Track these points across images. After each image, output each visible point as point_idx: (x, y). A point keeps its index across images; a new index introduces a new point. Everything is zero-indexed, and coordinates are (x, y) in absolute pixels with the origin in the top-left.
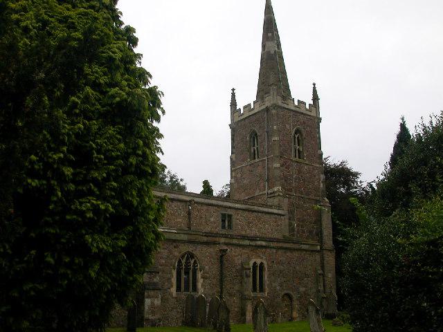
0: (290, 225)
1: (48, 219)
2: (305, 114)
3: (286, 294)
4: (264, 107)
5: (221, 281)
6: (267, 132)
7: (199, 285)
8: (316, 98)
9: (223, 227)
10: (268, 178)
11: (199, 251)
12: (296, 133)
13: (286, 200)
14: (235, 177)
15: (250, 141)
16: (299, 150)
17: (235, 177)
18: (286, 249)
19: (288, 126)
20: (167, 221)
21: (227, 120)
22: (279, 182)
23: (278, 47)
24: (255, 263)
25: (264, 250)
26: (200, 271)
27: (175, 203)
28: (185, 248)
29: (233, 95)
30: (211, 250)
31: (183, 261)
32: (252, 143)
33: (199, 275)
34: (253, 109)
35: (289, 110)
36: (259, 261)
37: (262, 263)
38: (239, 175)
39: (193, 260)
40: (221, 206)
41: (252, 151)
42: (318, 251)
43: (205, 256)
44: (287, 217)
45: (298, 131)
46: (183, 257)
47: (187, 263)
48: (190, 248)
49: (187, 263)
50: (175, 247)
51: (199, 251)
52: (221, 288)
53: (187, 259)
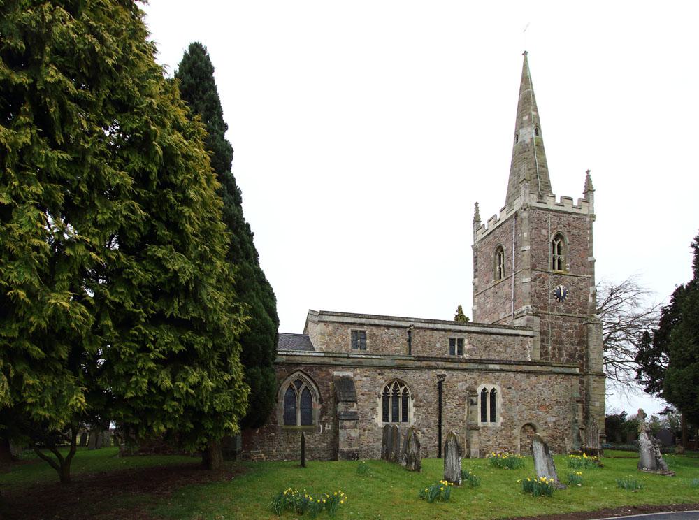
0: (543, 347)
1: (121, 413)
2: (570, 213)
3: (528, 424)
4: (512, 213)
5: (440, 400)
6: (515, 243)
7: (411, 415)
8: (589, 190)
9: (452, 352)
10: (515, 297)
11: (411, 377)
12: (556, 239)
13: (537, 320)
14: (478, 303)
15: (495, 259)
16: (559, 261)
17: (478, 303)
18: (529, 372)
19: (544, 232)
20: (382, 350)
21: (470, 241)
22: (529, 300)
23: (537, 134)
24: (485, 389)
25: (498, 374)
26: (412, 399)
27: (391, 330)
28: (391, 374)
29: (477, 209)
30: (426, 375)
31: (391, 390)
32: (497, 261)
33: (411, 403)
34: (487, 230)
35: (548, 210)
36: (489, 388)
37: (494, 390)
38: (482, 300)
39: (403, 388)
40: (450, 330)
41: (498, 270)
42: (577, 375)
43: (419, 381)
44: (538, 338)
45: (558, 236)
46: (389, 385)
47: (395, 391)
48: (399, 375)
49: (395, 391)
50: (379, 374)
51: (362, 380)
52: (440, 417)
53: (396, 386)
